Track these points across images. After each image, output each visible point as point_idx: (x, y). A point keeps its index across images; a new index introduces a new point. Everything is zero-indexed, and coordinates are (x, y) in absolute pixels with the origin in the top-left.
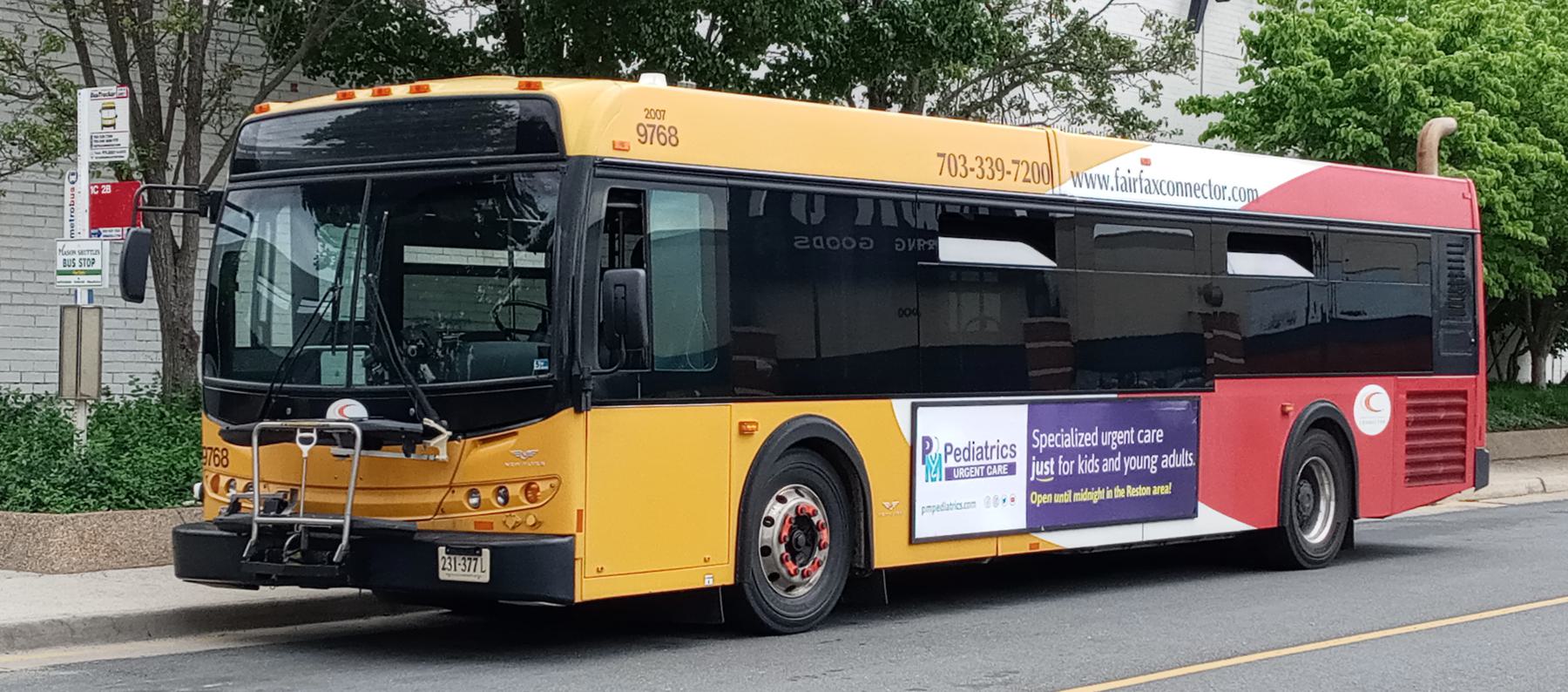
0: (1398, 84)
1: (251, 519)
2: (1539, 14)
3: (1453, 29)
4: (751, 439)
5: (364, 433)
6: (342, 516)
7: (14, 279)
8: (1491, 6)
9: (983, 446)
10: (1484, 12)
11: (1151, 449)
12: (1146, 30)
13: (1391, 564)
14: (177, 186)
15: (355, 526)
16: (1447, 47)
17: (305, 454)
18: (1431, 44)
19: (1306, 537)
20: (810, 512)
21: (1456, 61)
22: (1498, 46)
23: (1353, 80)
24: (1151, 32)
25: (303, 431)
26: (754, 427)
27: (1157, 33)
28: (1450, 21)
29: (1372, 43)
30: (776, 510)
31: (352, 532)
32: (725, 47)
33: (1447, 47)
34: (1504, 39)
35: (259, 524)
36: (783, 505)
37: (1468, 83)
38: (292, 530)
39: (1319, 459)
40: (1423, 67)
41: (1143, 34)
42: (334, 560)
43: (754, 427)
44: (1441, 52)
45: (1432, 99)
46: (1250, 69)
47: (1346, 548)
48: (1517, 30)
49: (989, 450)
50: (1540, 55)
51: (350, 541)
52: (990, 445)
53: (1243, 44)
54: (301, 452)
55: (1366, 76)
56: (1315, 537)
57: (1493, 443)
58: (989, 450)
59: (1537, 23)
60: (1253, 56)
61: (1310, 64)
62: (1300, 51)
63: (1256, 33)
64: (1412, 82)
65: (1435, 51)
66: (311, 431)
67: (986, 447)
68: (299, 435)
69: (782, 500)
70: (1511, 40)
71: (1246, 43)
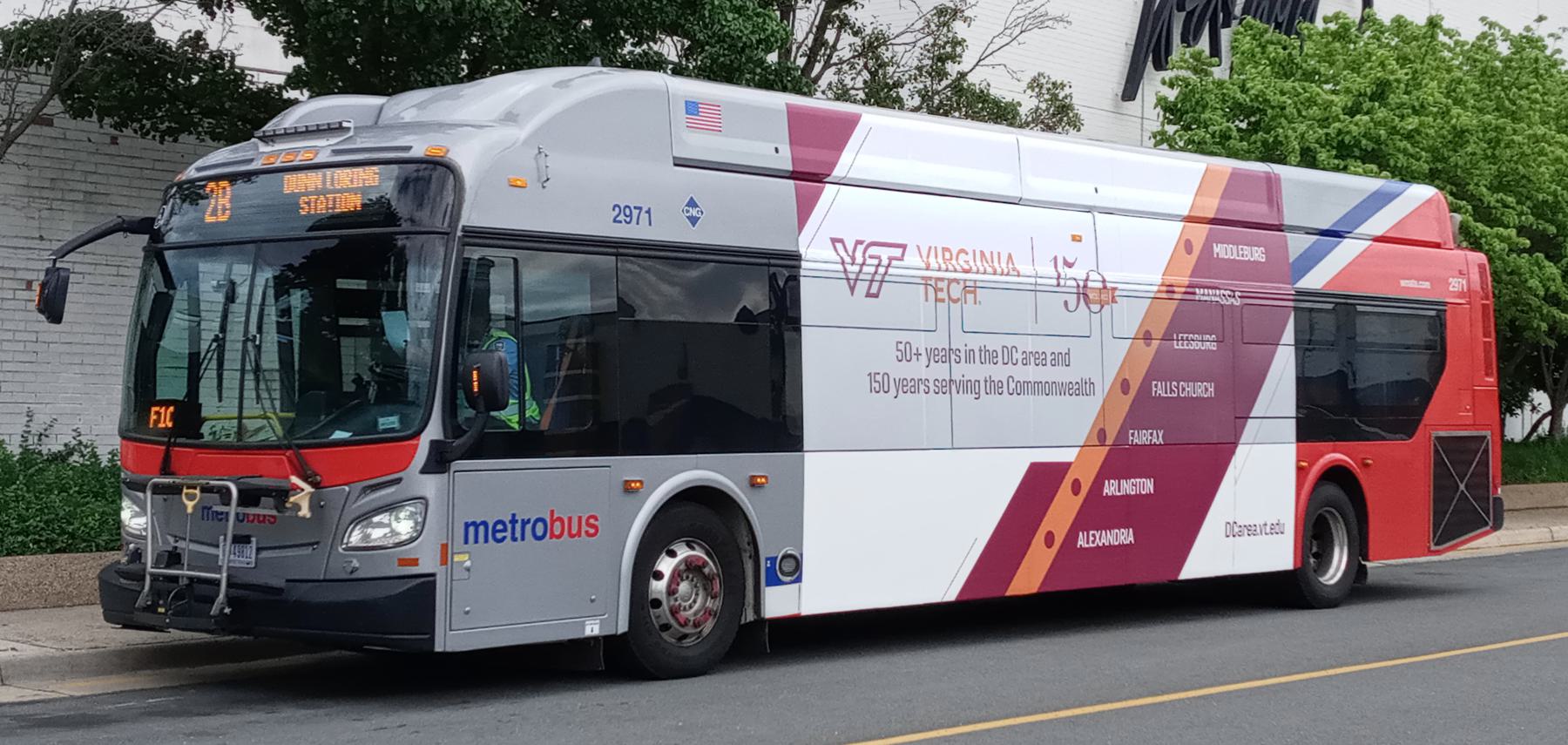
0: (1297, 147)
1: (144, 570)
2: (1460, 81)
3: (1360, 95)
4: (762, 491)
5: (240, 491)
6: (220, 573)
7: (16, 338)
8: (1400, 72)
9: (507, 519)
10: (1392, 78)
11: (225, 540)
12: (1029, 91)
13: (1419, 604)
14: (947, 298)
15: (234, 580)
16: (1352, 111)
17: (190, 510)
18: (1337, 110)
19: (1321, 579)
20: (700, 563)
21: (1356, 124)
22: (1410, 111)
23: (1259, 144)
24: (1034, 94)
25: (188, 488)
26: (763, 480)
27: (1039, 95)
28: (1357, 87)
29: (1273, 108)
30: (666, 565)
31: (229, 585)
32: (94, 50)
33: (1352, 111)
34: (1416, 104)
35: (152, 575)
36: (671, 559)
37: (1376, 147)
38: (178, 582)
39: (1333, 510)
40: (1325, 130)
41: (1026, 97)
42: (212, 613)
43: (763, 480)
44: (1347, 117)
45: (1336, 162)
46: (1163, 133)
47: (1358, 588)
48: (1429, 95)
49: (518, 526)
50: (1454, 121)
51: (227, 595)
52: (518, 518)
53: (1159, 109)
54: (185, 507)
55: (1271, 140)
56: (1331, 578)
57: (1509, 494)
58: (518, 526)
59: (1458, 90)
60: (1170, 122)
61: (1216, 128)
62: (1206, 115)
63: (1172, 99)
64: (1313, 146)
65: (1342, 117)
66: (195, 488)
67: (514, 521)
68: (185, 491)
69: (672, 554)
70: (1422, 106)
71: (1162, 107)
